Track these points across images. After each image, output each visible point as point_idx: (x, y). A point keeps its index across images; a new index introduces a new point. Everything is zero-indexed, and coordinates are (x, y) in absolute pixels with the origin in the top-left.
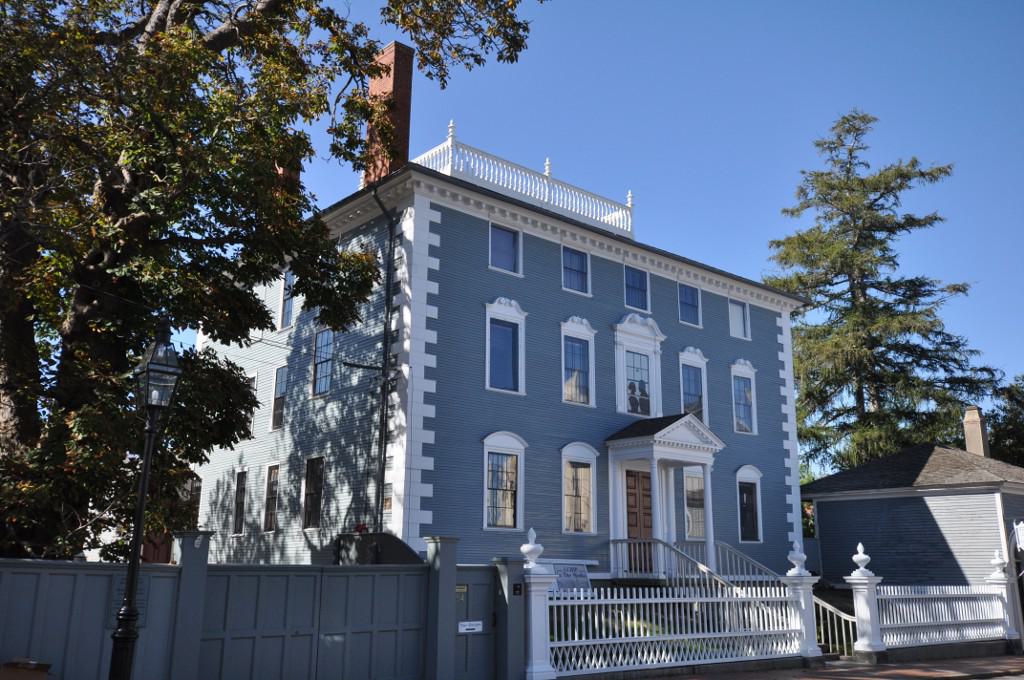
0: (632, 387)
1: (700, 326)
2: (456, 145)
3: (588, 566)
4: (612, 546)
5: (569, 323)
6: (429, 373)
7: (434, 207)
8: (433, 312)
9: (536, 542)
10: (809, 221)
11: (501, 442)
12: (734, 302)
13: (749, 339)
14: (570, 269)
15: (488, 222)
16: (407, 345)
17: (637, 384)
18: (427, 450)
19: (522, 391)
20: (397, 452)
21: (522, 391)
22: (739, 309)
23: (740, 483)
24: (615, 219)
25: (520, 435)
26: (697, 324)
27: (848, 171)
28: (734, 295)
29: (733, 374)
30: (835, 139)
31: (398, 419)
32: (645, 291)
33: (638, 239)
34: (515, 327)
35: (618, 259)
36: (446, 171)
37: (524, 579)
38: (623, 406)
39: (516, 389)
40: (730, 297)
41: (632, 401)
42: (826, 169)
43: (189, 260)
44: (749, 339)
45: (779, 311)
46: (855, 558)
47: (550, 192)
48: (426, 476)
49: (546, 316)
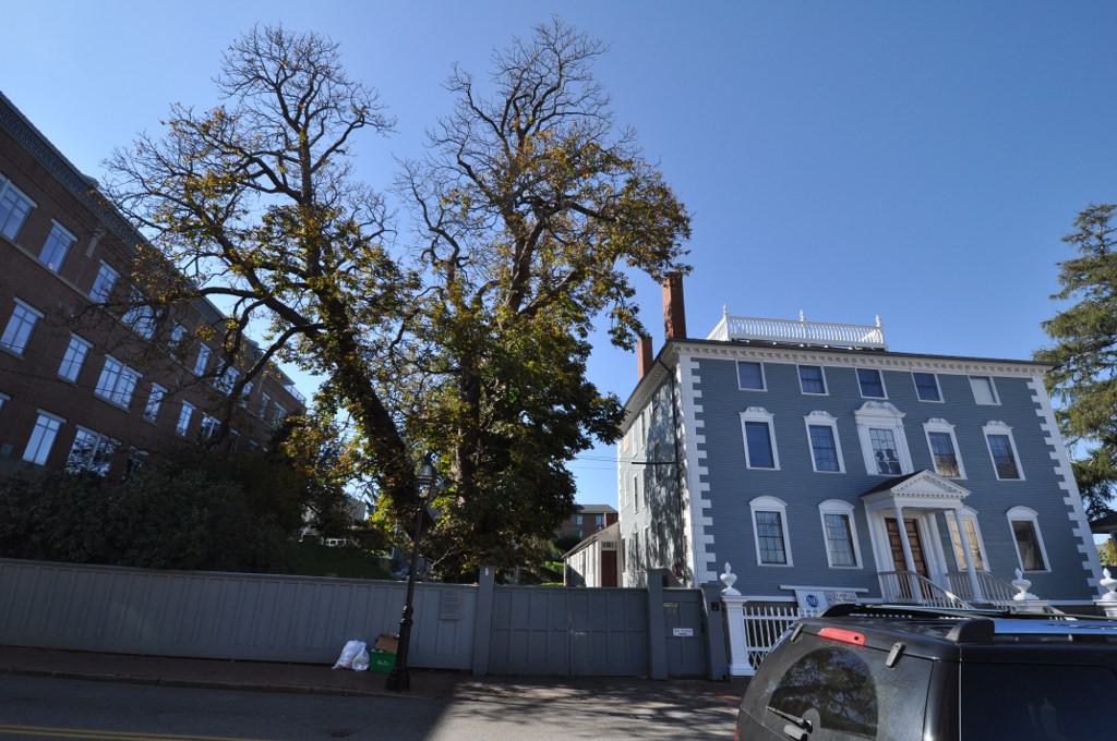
0: (879, 454)
1: (942, 401)
2: (730, 319)
3: (857, 593)
4: (880, 578)
5: (988, 425)
6: (702, 462)
7: (693, 360)
8: (701, 424)
9: (732, 572)
10: (1079, 297)
11: (764, 504)
12: (972, 377)
13: (999, 403)
14: (807, 380)
15: (795, 366)
16: (685, 447)
17: (884, 453)
18: (706, 512)
19: (777, 467)
20: (687, 515)
21: (777, 467)
22: (984, 383)
23: (1013, 522)
24: (873, 337)
25: (775, 496)
26: (939, 399)
27: (1102, 252)
28: (972, 371)
29: (986, 433)
30: (1080, 231)
31: (686, 495)
32: (936, 387)
33: (890, 349)
34: (766, 424)
35: (791, 362)
36: (724, 338)
37: (721, 599)
38: (872, 468)
39: (773, 466)
40: (969, 375)
41: (882, 464)
42: (1080, 256)
43: (156, 387)
44: (999, 403)
45: (1029, 377)
46: (1103, 582)
47: (807, 332)
48: (708, 530)
49: (790, 412)
